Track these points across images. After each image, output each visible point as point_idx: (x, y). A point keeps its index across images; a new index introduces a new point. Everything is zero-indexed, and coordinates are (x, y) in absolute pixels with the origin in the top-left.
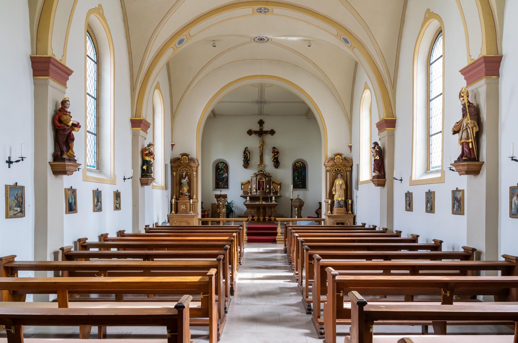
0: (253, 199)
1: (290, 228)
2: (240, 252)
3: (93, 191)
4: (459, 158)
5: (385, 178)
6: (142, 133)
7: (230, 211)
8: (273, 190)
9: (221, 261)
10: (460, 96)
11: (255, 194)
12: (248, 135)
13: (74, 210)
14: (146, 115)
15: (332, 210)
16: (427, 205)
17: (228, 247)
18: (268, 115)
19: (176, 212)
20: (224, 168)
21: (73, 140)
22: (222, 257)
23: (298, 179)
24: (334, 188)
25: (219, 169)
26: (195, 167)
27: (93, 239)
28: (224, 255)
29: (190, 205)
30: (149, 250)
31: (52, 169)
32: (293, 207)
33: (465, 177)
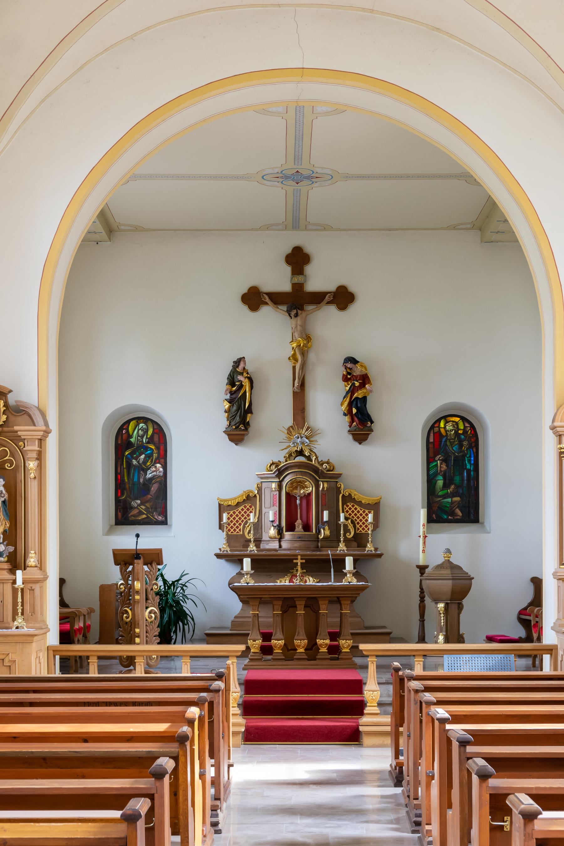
1: (415, 684)
2: (215, 782)
7: (173, 618)
8: (346, 530)
9: (141, 825)
12: (245, 308)
17: (168, 763)
18: (325, 228)
20: (151, 440)
22: (141, 805)
23: (445, 486)
25: (129, 445)
28: (151, 797)
29: (15, 591)
32: (428, 600)
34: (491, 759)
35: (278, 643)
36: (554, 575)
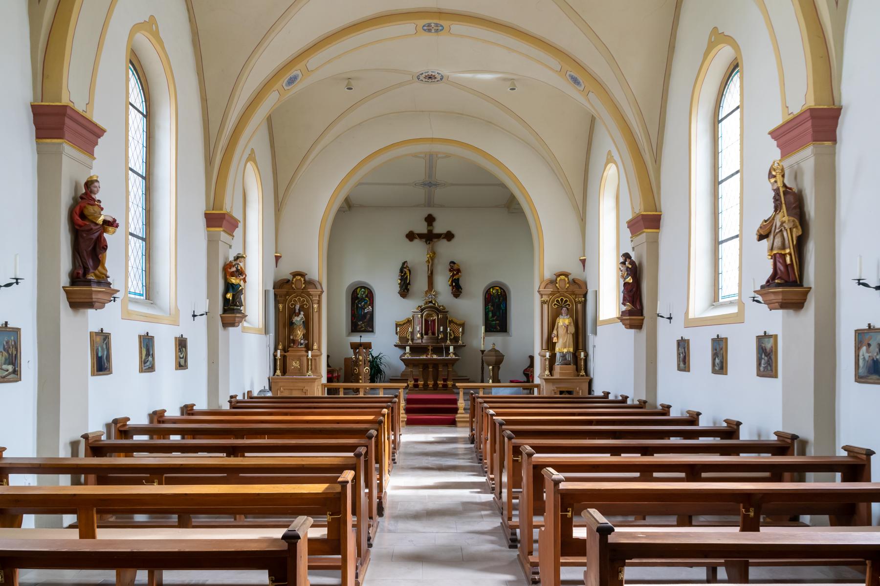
0: (415, 349)
1: (480, 400)
2: (394, 442)
3: (140, 337)
4: (768, 281)
5: (642, 315)
6: (224, 236)
7: (376, 372)
8: (450, 335)
9: (362, 458)
10: (771, 176)
11: (420, 341)
13: (106, 369)
14: (231, 206)
15: (551, 370)
18: (442, 206)
19: (284, 372)
20: (367, 296)
21: (105, 248)
22: (363, 450)
23: (493, 316)
24: (555, 332)
25: (358, 298)
27: (139, 418)
28: (367, 447)
29: (308, 360)
31: (68, 298)
34: (513, 431)
36: (539, 354)
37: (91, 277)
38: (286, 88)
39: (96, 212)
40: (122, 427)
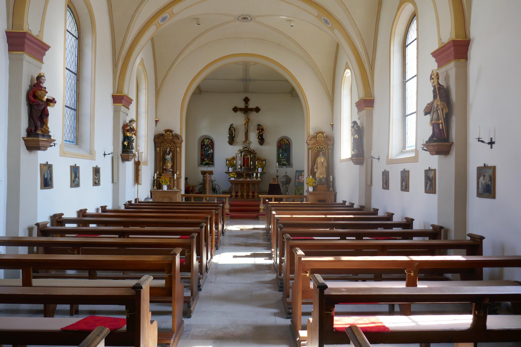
0: (239, 175)
3: (71, 167)
4: (429, 139)
6: (123, 109)
10: (431, 78)
11: (240, 170)
12: (233, 112)
13: (49, 185)
16: (402, 183)
20: (210, 144)
21: (47, 115)
23: (282, 156)
24: (316, 166)
26: (178, 143)
27: (70, 213)
30: (106, 226)
31: (25, 144)
33: (436, 157)
35: (239, 194)
37: (39, 132)
38: (160, 23)
39: (42, 94)
40: (58, 219)
